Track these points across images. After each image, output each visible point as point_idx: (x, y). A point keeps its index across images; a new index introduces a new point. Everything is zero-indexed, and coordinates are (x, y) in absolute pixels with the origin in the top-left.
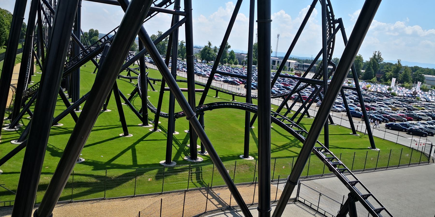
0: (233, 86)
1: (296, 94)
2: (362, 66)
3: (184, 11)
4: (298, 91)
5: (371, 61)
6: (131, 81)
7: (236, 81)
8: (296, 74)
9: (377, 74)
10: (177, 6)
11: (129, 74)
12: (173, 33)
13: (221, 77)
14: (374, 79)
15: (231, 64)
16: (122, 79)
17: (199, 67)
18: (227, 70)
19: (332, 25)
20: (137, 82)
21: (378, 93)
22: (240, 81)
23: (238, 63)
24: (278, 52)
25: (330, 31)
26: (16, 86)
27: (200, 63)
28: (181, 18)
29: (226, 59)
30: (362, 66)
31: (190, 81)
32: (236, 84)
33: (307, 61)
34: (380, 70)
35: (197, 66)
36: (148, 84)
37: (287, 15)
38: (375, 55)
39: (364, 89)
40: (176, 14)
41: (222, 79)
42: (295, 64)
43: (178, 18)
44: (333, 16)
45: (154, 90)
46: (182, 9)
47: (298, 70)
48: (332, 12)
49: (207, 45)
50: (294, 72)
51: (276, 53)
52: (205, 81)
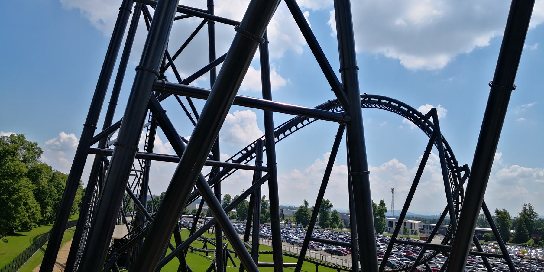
0: (338, 257)
1: (423, 266)
2: (511, 224)
3: (266, 166)
4: (425, 262)
5: (522, 218)
6: (207, 255)
7: (343, 250)
8: (421, 238)
9: (533, 235)
10: (259, 161)
11: (205, 246)
12: (255, 191)
13: (322, 246)
14: (530, 241)
15: (335, 227)
16: (197, 252)
17: (293, 233)
18: (330, 236)
19: (456, 174)
20: (213, 256)
21: (539, 260)
22: (348, 250)
23: (344, 226)
24: (395, 210)
25: (455, 181)
26: (65, 265)
27: (295, 228)
28: (264, 174)
29: (328, 222)
30: (511, 224)
31: (277, 252)
32: (342, 254)
33: (434, 221)
34: (536, 229)
35: (291, 232)
36: (228, 258)
37: (401, 164)
38: (525, 210)
39: (519, 256)
40: (257, 170)
41: (324, 249)
42: (419, 226)
43: (260, 174)
44: (456, 163)
45: (235, 266)
46: (265, 164)
47: (424, 232)
48: (453, 157)
49: (302, 204)
50: (419, 235)
51: (393, 211)
52: (297, 250)
